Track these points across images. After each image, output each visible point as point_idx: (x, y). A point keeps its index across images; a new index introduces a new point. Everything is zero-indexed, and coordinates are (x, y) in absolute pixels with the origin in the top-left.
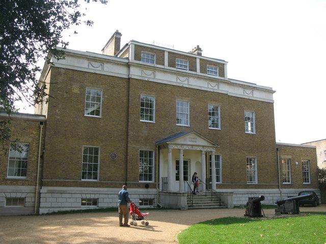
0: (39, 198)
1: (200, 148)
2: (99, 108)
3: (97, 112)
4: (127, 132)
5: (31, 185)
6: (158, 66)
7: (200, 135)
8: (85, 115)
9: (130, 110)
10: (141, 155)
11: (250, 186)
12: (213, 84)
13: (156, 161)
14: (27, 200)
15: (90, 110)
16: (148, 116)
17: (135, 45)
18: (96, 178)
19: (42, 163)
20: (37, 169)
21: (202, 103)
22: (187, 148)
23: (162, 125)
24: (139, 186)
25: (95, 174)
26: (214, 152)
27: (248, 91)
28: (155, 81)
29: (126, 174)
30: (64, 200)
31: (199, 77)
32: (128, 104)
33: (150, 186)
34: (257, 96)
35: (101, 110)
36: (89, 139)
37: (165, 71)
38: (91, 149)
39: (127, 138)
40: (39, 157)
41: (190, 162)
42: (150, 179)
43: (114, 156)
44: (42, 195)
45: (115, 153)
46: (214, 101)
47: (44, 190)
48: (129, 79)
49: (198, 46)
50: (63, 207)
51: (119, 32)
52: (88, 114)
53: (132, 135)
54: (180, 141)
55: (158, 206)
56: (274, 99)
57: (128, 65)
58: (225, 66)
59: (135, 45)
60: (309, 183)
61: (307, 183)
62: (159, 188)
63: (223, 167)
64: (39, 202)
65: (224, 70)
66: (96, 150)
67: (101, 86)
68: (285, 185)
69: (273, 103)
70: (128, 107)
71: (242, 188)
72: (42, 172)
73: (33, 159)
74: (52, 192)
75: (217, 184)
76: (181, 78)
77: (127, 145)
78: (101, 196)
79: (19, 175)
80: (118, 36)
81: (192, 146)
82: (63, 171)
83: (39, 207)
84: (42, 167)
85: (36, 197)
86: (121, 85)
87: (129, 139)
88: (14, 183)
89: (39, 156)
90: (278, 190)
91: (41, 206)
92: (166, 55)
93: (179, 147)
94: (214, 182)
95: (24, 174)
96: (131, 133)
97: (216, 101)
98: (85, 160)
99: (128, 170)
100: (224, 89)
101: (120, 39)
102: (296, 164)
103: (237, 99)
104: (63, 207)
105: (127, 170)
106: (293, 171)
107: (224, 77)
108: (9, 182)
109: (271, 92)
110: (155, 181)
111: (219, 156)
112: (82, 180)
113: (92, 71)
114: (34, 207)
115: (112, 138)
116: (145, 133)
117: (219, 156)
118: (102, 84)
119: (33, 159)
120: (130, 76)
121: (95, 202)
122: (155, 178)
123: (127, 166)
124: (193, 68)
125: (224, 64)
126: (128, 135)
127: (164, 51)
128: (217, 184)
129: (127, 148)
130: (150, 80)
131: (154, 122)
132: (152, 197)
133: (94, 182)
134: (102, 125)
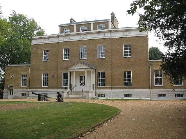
12: (101, 35)
27: (127, 33)
28: (87, 39)
37: (74, 35)
59: (76, 25)
76: (83, 36)
93: (73, 70)
97: (102, 43)
121: (130, 96)
127: (108, 22)
130: (67, 41)
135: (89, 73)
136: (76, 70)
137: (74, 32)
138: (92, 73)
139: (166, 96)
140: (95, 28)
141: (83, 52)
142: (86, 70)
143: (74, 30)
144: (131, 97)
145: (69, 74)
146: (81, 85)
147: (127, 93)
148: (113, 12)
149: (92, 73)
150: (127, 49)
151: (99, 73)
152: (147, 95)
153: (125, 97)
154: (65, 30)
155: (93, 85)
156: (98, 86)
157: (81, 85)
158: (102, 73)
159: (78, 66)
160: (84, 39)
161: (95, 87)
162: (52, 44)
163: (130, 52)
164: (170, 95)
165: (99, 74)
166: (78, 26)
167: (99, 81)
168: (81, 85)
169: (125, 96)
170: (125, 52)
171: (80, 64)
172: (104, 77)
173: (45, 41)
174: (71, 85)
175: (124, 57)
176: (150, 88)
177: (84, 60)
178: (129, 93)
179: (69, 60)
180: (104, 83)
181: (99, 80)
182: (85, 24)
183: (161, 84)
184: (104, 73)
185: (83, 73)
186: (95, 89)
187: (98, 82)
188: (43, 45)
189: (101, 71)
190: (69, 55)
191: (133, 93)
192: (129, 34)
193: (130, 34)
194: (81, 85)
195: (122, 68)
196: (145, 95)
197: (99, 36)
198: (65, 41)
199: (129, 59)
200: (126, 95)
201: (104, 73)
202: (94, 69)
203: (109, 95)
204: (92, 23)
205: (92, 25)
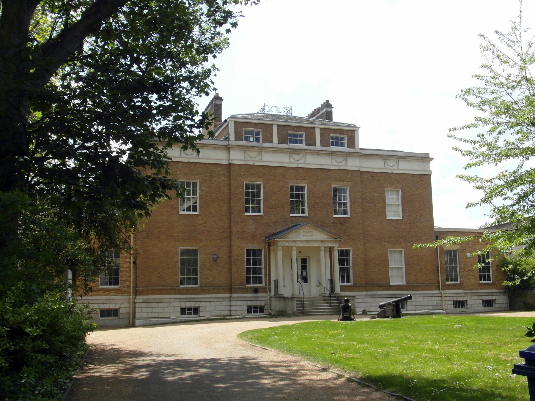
0: (135, 308)
1: (319, 244)
2: (196, 202)
3: (194, 208)
4: (230, 228)
5: (124, 295)
6: (265, 145)
7: (320, 226)
8: (181, 213)
9: (232, 202)
10: (248, 255)
11: (393, 288)
12: (339, 159)
13: (265, 260)
14: (122, 311)
15: (186, 205)
16: (190, 278)
17: (235, 122)
18: (196, 284)
19: (135, 269)
20: (130, 276)
21: (324, 185)
22: (301, 245)
23: (272, 216)
24: (246, 290)
25: (195, 280)
26: (336, 247)
27: (391, 163)
28: (262, 164)
29: (231, 278)
30: (161, 310)
31: (319, 153)
32: (230, 195)
33: (259, 291)
34: (405, 167)
35: (198, 205)
36: (186, 239)
37: (274, 150)
38: (189, 251)
39: (230, 236)
40: (132, 264)
41: (309, 260)
42: (260, 282)
43: (215, 258)
44: (137, 305)
45: (217, 253)
46: (340, 181)
47: (140, 298)
48: (230, 164)
49: (327, 101)
50: (160, 318)
51: (220, 96)
52: (184, 210)
53: (235, 232)
54: (292, 236)
55: (270, 314)
56: (431, 169)
57: (228, 148)
58: (356, 133)
59: (235, 122)
60: (491, 282)
61: (487, 282)
62: (270, 292)
63: (353, 264)
64: (134, 313)
65: (354, 138)
66: (195, 251)
67: (197, 177)
68: (449, 285)
69: (430, 175)
70: (230, 199)
71: (382, 290)
72: (135, 279)
73: (125, 266)
74: (146, 302)
75: (341, 286)
76: (296, 157)
77: (230, 243)
78: (202, 304)
79: (111, 284)
80: (218, 102)
81: (308, 241)
82: (159, 277)
83: (134, 317)
84: (135, 274)
85: (131, 307)
86: (220, 173)
87: (233, 237)
88: (107, 293)
89: (132, 261)
90: (437, 292)
91: (136, 317)
92: (275, 129)
93: (291, 244)
94: (338, 284)
95: (117, 282)
96: (234, 229)
97: (343, 181)
98: (183, 264)
99: (233, 273)
100: (353, 164)
101: (221, 105)
102: (467, 256)
103: (374, 175)
104: (160, 318)
105: (231, 273)
106: (462, 266)
107: (354, 148)
108: (101, 292)
109: (425, 158)
110: (266, 285)
111: (349, 250)
112: (181, 286)
113: (186, 160)
114: (130, 318)
115: (213, 237)
116: (251, 227)
117: (349, 250)
118: (198, 175)
119: (125, 266)
120: (231, 162)
121: (196, 311)
122: (266, 280)
123: (231, 269)
124: (311, 142)
125: (354, 131)
126: (230, 232)
127: (272, 125)
128: (341, 286)
129: (230, 247)
130: (256, 164)
131: (262, 214)
132: (263, 303)
133: (194, 288)
134: (200, 222)
136: (298, 244)
138: (323, 253)
147: (188, 305)
148: (327, 105)
149: (323, 253)
150: (298, 197)
152: (435, 303)
153: (182, 314)
159: (304, 234)
162: (208, 165)
164: (473, 302)
169: (183, 311)
173: (295, 162)
176: (439, 289)
187: (263, 276)
188: (180, 164)
192: (302, 161)
193: (398, 166)
196: (432, 303)
197: (292, 160)
198: (251, 163)
205: (275, 129)
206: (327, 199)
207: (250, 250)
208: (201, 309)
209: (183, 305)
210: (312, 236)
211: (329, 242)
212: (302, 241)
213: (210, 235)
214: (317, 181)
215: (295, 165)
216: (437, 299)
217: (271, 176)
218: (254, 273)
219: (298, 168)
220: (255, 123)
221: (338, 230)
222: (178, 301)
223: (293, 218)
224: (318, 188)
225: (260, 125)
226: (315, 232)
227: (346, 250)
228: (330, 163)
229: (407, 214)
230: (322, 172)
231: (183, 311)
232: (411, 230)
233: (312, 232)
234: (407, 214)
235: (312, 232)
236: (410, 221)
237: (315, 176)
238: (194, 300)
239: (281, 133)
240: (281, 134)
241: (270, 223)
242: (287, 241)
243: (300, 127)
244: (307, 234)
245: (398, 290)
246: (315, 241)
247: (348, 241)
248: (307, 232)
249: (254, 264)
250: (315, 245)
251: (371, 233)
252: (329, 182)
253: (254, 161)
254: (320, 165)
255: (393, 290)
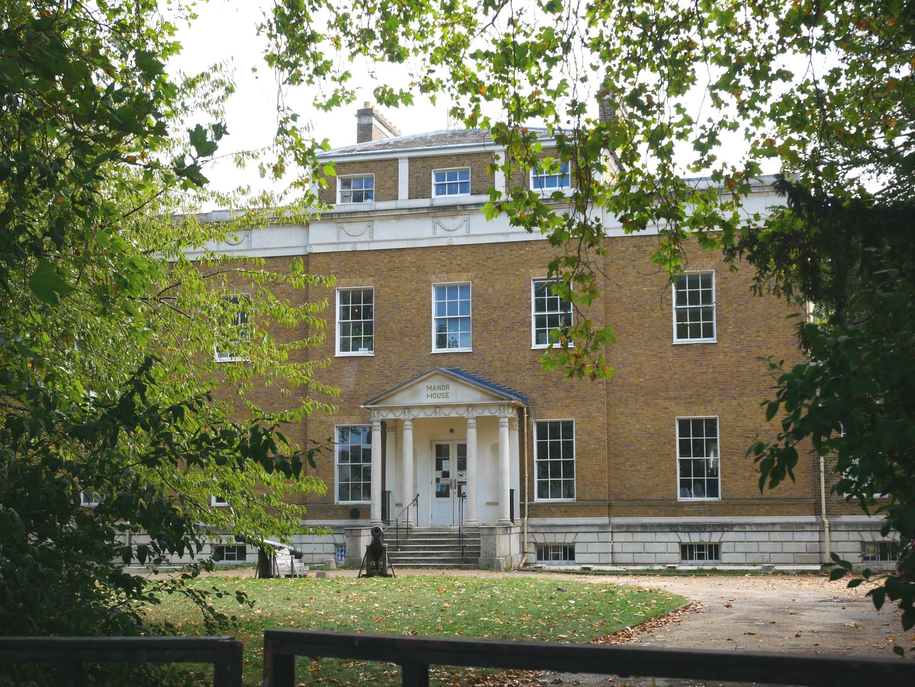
1: (462, 412)
18: (570, 495)
21: (512, 278)
23: (393, 356)
37: (399, 215)
59: (410, 159)
71: (656, 515)
76: (448, 222)
90: (812, 519)
92: (404, 169)
93: (399, 415)
127: (397, 160)
130: (360, 247)
133: (710, 504)
135: (488, 426)
137: (396, 198)
139: (576, 556)
140: (419, 189)
141: (453, 310)
142: (475, 415)
143: (396, 186)
144: (717, 558)
145: (377, 436)
146: (443, 493)
149: (505, 432)
150: (694, 299)
151: (541, 427)
152: (802, 548)
153: (684, 557)
154: (440, 177)
155: (512, 491)
156: (537, 500)
157: (443, 493)
158: (555, 426)
159: (430, 392)
160: (456, 242)
161: (522, 507)
163: (708, 315)
165: (542, 434)
166: (420, 164)
167: (543, 473)
168: (439, 495)
169: (686, 551)
170: (681, 316)
171: (436, 381)
172: (568, 447)
173: (446, 234)
174: (385, 495)
175: (676, 341)
176: (817, 512)
177: (459, 358)
178: (560, 539)
179: (370, 354)
180: (569, 486)
181: (542, 466)
182: (458, 155)
183: (713, 492)
184: (568, 427)
185: (456, 426)
186: (522, 516)
187: (536, 480)
189: (552, 417)
190: (369, 328)
191: (728, 536)
193: (249, 243)
194: (439, 495)
195: (665, 403)
196: (793, 548)
197: (440, 232)
198: (349, 248)
199: (703, 354)
200: (547, 548)
201: (568, 427)
202: (514, 406)
203: (597, 548)
204: (404, 158)
205: (404, 169)
206: (517, 311)
207: (688, 421)
208: (723, 548)
209: (685, 538)
210: (447, 396)
211: (485, 406)
212: (422, 407)
213: (271, 401)
214: (495, 272)
215: (443, 242)
216: (807, 536)
217: (392, 270)
218: (555, 474)
219: (452, 246)
220: (361, 162)
221: (542, 378)
222: (597, 529)
223: (438, 358)
224: (498, 287)
225: (372, 165)
226: (453, 387)
227: (708, 421)
228: (366, 237)
229: (731, 329)
230: (506, 250)
231: (686, 551)
232: (742, 369)
233: (448, 387)
234: (731, 329)
235: (448, 387)
236: (739, 347)
237: (490, 261)
238: (574, 530)
239: (417, 175)
240: (418, 177)
241: (386, 371)
242: (391, 409)
243: (458, 156)
244: (437, 392)
245: (700, 514)
246: (454, 406)
247: (568, 401)
248: (435, 388)
249: (699, 452)
250: (454, 414)
251: (631, 380)
252: (523, 270)
253: (355, 243)
254: (503, 234)
255: (687, 514)
